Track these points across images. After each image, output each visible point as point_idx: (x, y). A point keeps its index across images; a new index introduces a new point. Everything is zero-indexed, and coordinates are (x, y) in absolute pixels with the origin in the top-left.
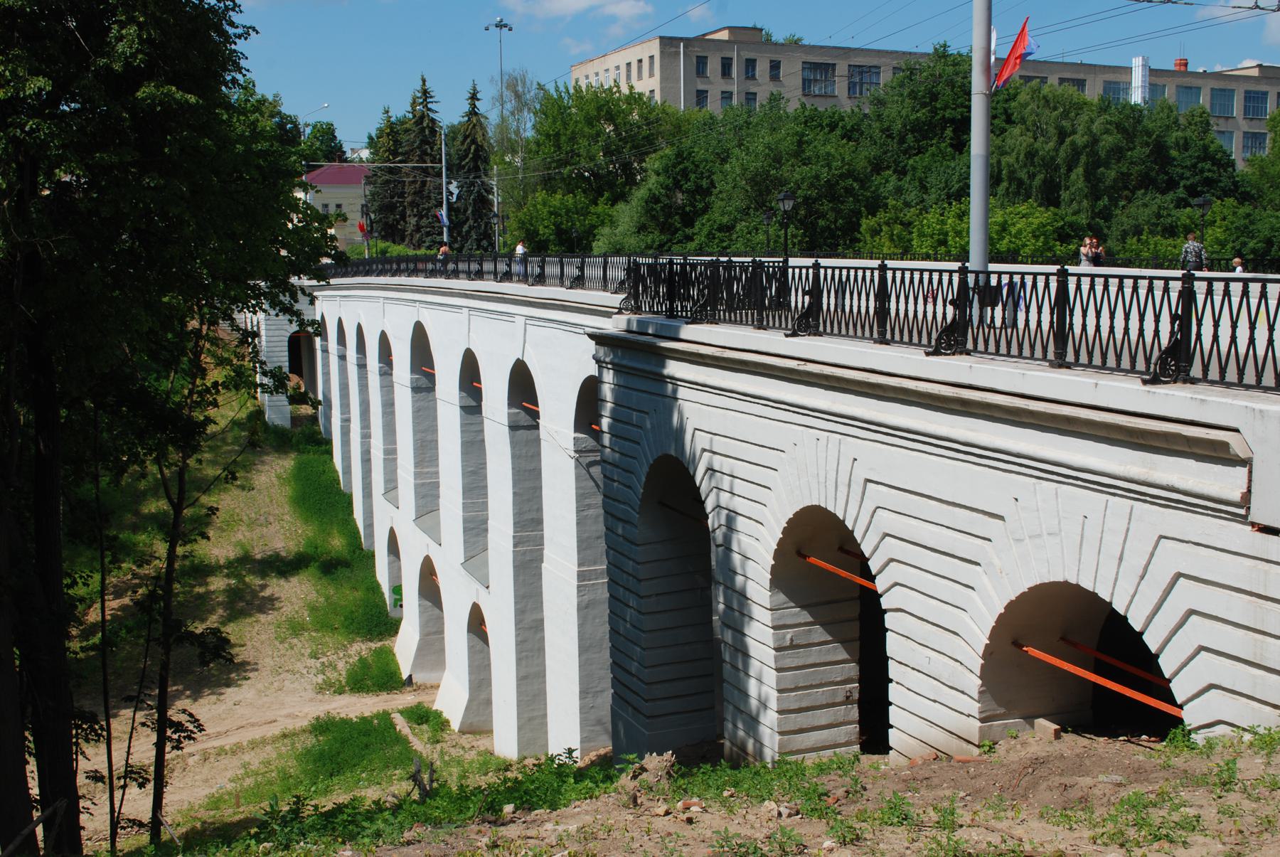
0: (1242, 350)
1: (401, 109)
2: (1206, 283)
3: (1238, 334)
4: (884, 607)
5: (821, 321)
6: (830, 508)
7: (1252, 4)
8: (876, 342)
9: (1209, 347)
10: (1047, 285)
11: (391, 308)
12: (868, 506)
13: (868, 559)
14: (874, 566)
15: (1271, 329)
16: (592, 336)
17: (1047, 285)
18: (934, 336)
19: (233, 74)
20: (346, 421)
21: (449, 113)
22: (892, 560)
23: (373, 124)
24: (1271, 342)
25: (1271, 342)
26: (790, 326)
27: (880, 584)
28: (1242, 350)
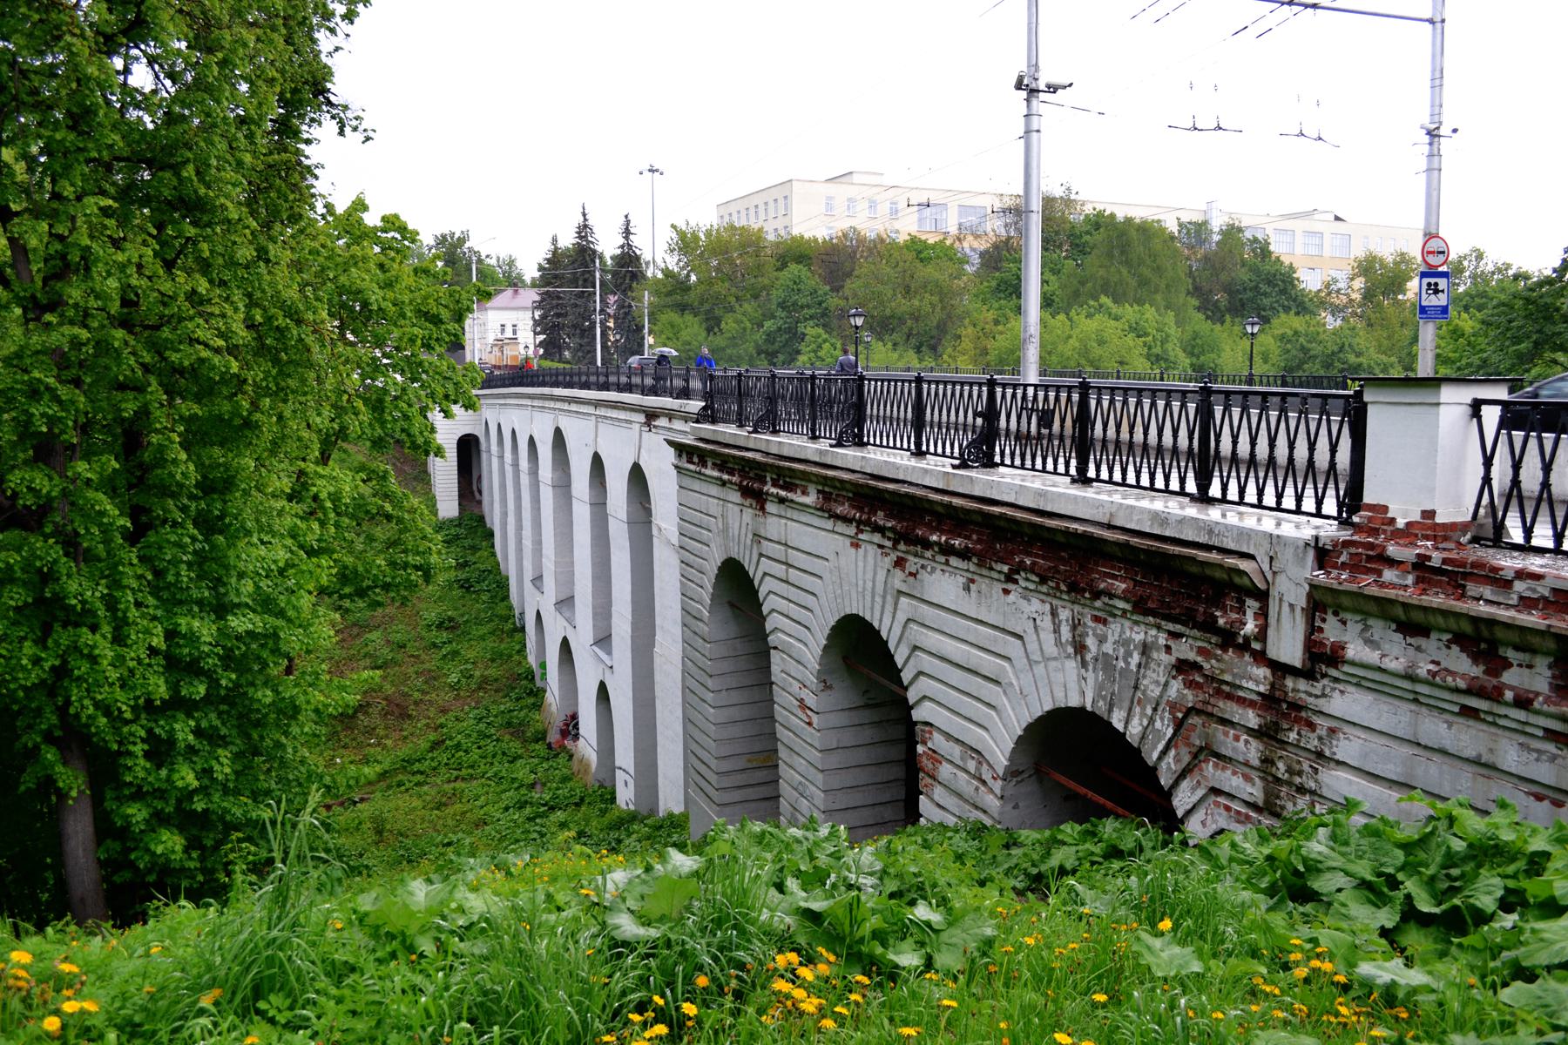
0: (1270, 483)
1: (567, 240)
2: (1499, 408)
3: (1287, 451)
4: (914, 719)
5: (997, 449)
6: (868, 618)
7: (1316, 136)
8: (1074, 481)
9: (1287, 490)
10: (1069, 398)
11: (537, 415)
12: (901, 617)
13: (901, 671)
14: (906, 676)
15: (1547, 468)
16: (671, 443)
17: (1069, 398)
18: (965, 443)
19: (141, 113)
20: (505, 514)
21: (608, 245)
22: (921, 673)
23: (541, 253)
24: (1488, 462)
25: (1488, 462)
26: (956, 454)
27: (912, 696)
28: (1270, 483)
